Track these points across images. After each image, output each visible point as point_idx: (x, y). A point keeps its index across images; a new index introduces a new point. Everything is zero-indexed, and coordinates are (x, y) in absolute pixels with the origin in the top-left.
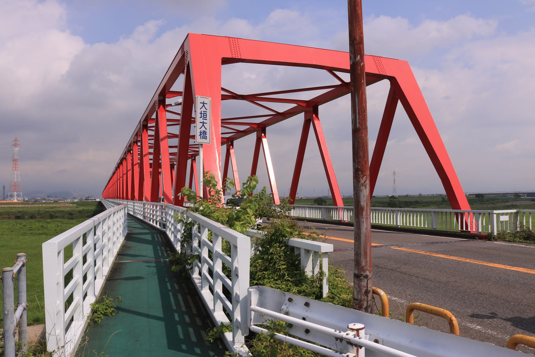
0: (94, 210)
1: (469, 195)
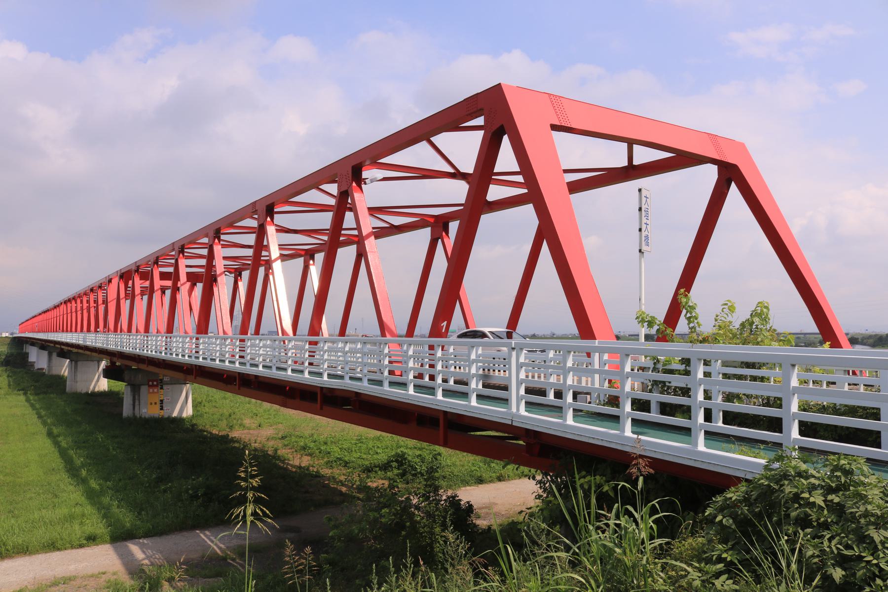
0: (6, 353)
1: (629, 335)
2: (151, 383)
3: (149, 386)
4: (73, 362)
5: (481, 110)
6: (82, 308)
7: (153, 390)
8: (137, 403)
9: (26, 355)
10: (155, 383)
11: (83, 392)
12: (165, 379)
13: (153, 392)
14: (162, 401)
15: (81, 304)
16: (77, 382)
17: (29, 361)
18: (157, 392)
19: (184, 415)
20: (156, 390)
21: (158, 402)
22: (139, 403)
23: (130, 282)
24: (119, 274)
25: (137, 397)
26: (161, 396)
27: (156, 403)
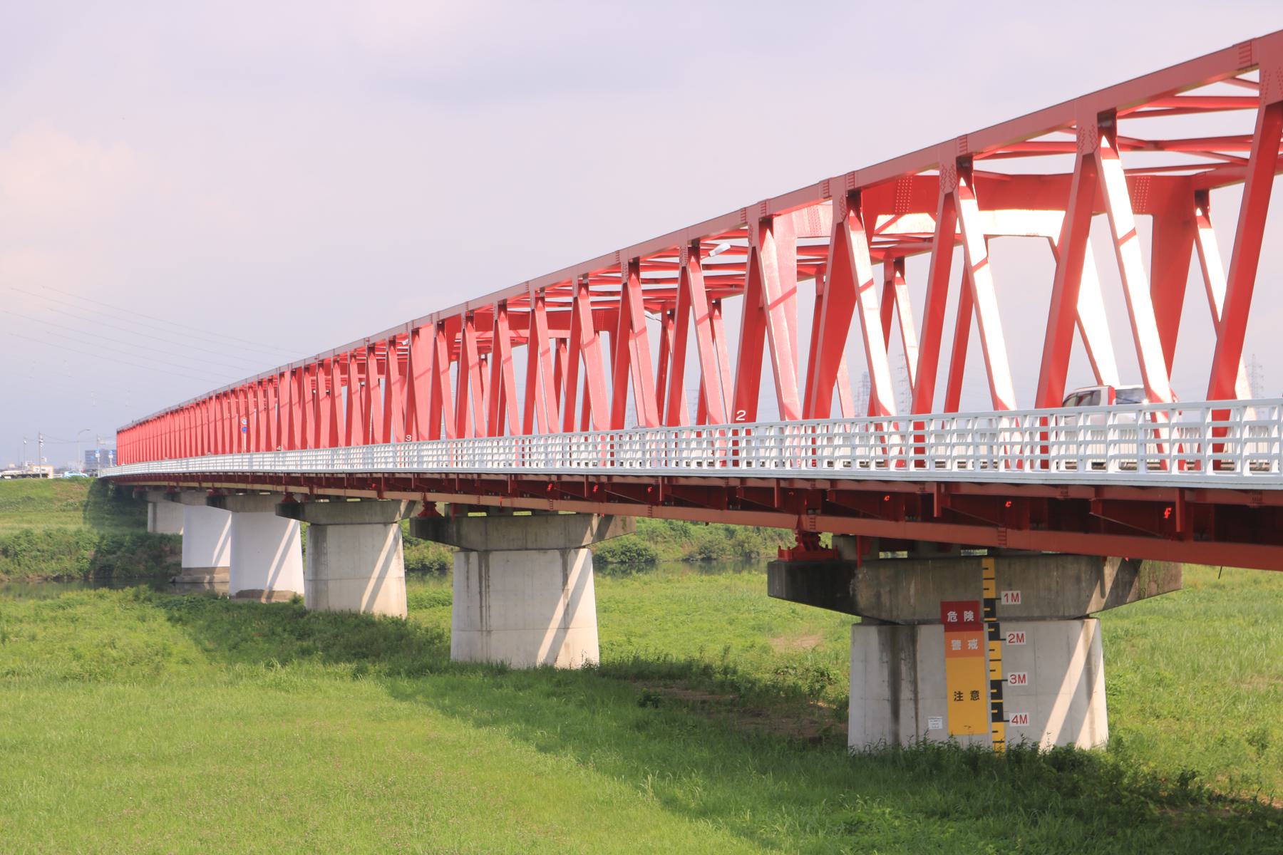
2: (952, 616)
3: (950, 627)
4: (474, 556)
5: (1257, 64)
6: (267, 404)
7: (964, 645)
8: (906, 694)
9: (166, 549)
10: (969, 616)
11: (574, 667)
12: (1004, 601)
13: (965, 652)
14: (997, 685)
15: (275, 397)
16: (489, 632)
17: (184, 565)
18: (980, 652)
19: (1084, 742)
20: (973, 644)
21: (986, 692)
22: (915, 692)
23: (459, 336)
24: (435, 321)
25: (904, 669)
26: (993, 665)
27: (975, 695)
